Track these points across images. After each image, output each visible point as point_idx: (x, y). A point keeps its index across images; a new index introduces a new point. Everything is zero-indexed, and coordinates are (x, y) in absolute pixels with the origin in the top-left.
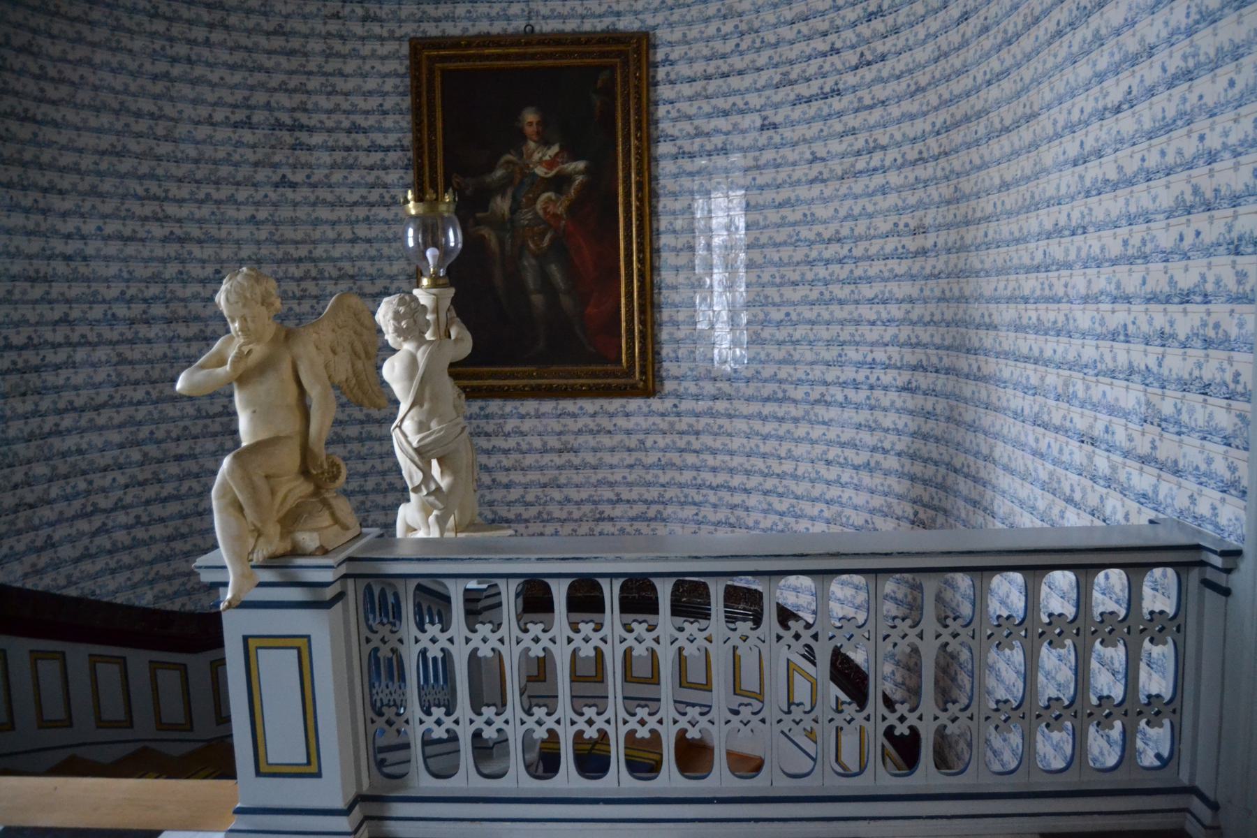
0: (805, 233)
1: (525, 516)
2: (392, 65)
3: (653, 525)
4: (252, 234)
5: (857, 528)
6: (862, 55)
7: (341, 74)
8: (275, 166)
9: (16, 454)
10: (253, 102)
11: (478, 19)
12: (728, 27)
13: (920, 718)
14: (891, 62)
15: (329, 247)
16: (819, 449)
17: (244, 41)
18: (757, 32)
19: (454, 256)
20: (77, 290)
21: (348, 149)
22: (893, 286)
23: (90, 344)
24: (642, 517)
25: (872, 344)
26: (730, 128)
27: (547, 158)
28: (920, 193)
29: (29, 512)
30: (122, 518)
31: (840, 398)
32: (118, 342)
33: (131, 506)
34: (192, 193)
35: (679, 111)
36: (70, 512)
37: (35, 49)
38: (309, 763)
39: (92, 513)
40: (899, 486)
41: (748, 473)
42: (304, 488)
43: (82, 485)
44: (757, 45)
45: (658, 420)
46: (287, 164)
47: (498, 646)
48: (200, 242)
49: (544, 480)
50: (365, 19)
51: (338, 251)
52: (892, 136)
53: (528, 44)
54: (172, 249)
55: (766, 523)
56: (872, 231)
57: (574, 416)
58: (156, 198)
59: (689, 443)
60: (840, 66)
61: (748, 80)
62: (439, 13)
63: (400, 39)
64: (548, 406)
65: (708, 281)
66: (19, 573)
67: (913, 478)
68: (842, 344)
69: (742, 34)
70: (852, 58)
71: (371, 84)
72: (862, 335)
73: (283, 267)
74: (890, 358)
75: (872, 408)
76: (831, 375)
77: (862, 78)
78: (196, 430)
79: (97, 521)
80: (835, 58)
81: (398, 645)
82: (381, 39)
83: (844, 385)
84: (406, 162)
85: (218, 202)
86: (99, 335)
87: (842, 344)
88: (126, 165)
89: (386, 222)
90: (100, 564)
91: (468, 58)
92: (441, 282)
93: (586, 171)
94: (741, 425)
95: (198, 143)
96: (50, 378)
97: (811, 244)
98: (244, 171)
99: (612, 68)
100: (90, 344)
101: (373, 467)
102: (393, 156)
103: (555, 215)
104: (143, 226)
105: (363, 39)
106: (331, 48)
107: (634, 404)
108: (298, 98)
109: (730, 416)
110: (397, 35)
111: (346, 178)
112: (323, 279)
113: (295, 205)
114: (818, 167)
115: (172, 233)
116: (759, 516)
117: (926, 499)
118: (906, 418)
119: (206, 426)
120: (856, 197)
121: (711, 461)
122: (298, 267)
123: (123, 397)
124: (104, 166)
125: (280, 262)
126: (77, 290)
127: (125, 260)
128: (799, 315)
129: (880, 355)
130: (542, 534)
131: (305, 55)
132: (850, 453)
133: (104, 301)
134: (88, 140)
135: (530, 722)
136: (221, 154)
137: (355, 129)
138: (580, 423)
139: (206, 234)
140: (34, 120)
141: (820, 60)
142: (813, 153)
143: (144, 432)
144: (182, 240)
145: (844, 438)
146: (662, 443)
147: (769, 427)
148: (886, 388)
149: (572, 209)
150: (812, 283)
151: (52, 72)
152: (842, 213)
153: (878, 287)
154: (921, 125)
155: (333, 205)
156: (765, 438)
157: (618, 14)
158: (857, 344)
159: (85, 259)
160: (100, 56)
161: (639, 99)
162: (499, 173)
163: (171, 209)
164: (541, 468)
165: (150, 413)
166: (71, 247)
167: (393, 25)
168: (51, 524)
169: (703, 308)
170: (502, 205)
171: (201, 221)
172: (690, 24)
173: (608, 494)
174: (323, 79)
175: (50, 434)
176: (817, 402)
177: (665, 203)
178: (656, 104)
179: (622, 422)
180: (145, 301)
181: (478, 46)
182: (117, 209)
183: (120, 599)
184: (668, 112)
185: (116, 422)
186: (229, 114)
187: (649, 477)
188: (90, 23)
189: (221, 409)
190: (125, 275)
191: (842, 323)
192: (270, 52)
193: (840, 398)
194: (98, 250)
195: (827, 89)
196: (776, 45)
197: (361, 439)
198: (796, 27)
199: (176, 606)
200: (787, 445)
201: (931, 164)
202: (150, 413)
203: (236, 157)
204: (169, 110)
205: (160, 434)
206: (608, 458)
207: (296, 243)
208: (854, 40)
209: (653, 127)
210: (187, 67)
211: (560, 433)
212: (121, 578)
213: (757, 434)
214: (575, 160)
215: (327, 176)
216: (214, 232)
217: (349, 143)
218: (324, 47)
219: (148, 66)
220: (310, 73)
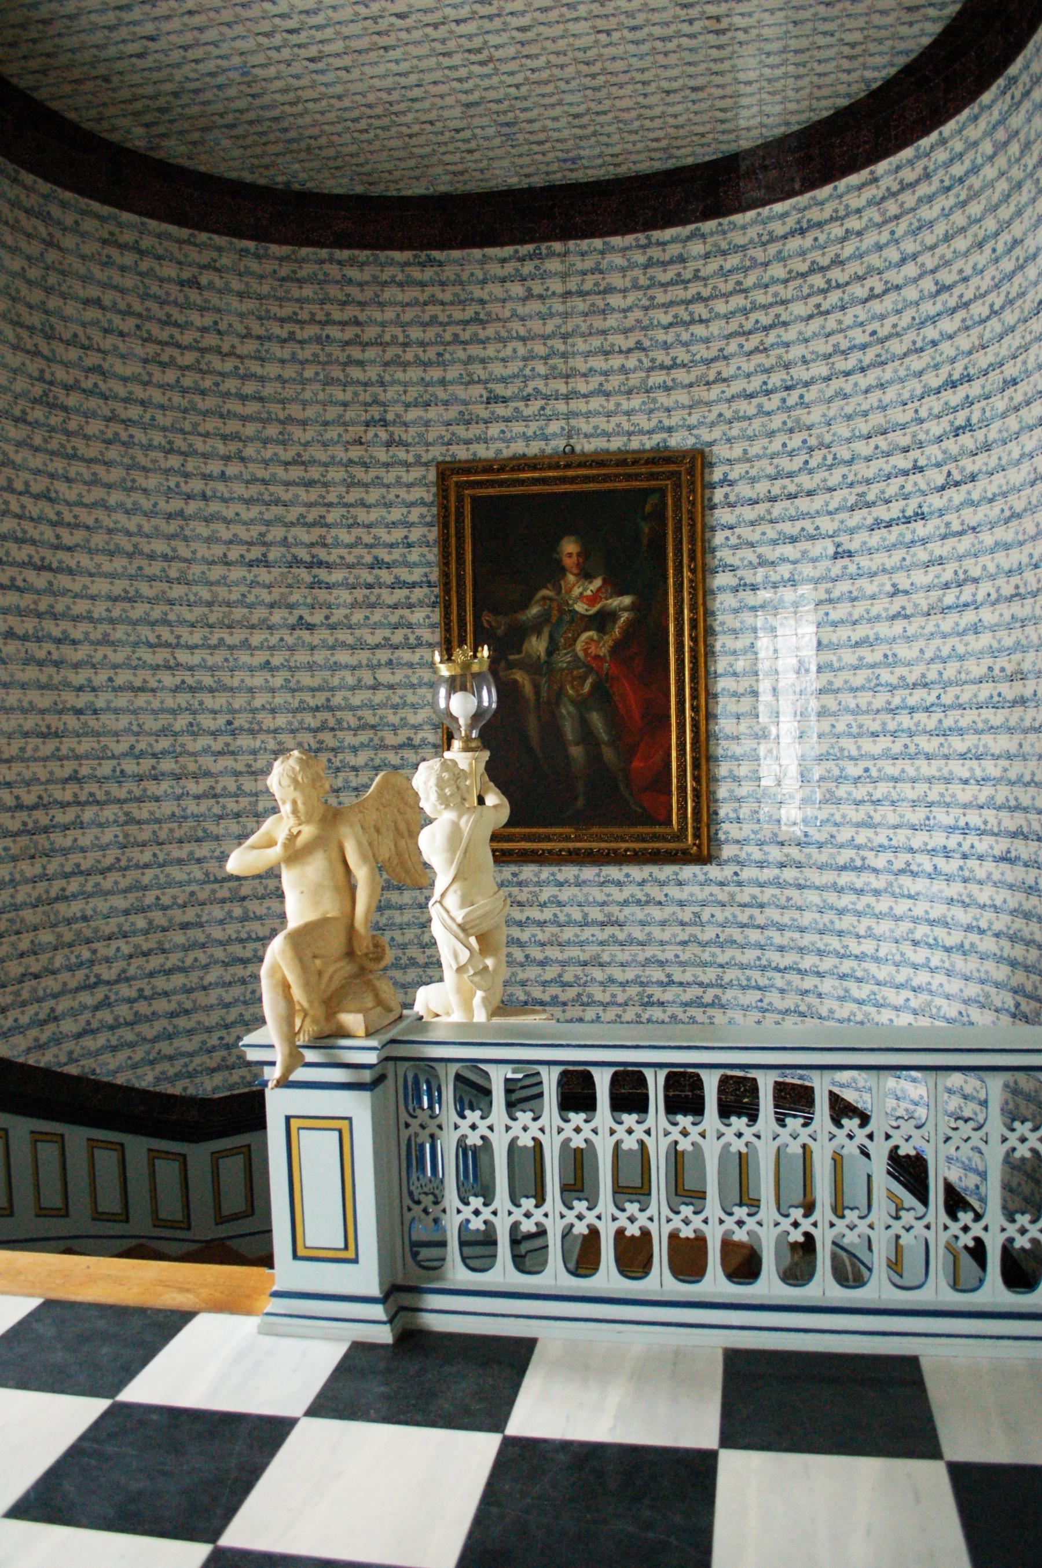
0: (886, 676)
1: (563, 998)
2: (418, 493)
3: (710, 1011)
5: (948, 1021)
6: (949, 474)
7: (363, 504)
8: (291, 607)
9: (23, 920)
10: (269, 538)
11: (512, 440)
12: (795, 442)
13: (986, 1229)
14: (982, 483)
15: (348, 694)
16: (905, 926)
17: (261, 473)
19: (488, 717)
20: (87, 745)
21: (369, 586)
22: (987, 739)
23: (98, 803)
24: (697, 1003)
25: (965, 806)
26: (799, 556)
28: (1017, 634)
29: (34, 982)
30: (125, 991)
31: (929, 868)
32: (125, 801)
33: (134, 978)
34: (205, 638)
36: (73, 984)
37: (53, 495)
38: (346, 1248)
39: (96, 985)
40: (1001, 973)
41: (820, 953)
42: (347, 969)
43: (86, 955)
44: (829, 462)
45: (715, 889)
48: (211, 690)
49: (583, 957)
52: (984, 568)
53: (568, 466)
55: (843, 1012)
56: (963, 676)
57: (619, 884)
58: (168, 645)
59: (751, 917)
60: (923, 486)
61: (818, 502)
62: (470, 435)
63: (426, 464)
64: (589, 872)
65: (773, 730)
66: (23, 1047)
67: (1013, 964)
68: (930, 805)
70: (938, 477)
71: (396, 514)
72: (953, 796)
73: (299, 716)
74: (985, 823)
75: (965, 881)
76: (918, 840)
77: (950, 500)
78: (203, 895)
79: (100, 993)
81: (437, 1131)
82: (407, 465)
83: (932, 852)
85: (231, 648)
86: (107, 793)
87: (930, 805)
88: (139, 611)
89: (411, 665)
90: (101, 1040)
91: (501, 483)
92: (474, 745)
94: (813, 897)
95: (212, 584)
96: (59, 839)
97: (893, 688)
100: (98, 803)
102: (418, 593)
103: (597, 657)
105: (387, 465)
106: (353, 477)
107: (688, 871)
109: (800, 887)
111: (367, 618)
113: (313, 648)
114: (900, 601)
115: (183, 682)
116: (835, 1005)
117: (1029, 988)
118: (1005, 893)
119: (213, 891)
120: (944, 636)
121: (778, 939)
123: (129, 860)
124: (116, 613)
125: (295, 711)
126: (87, 745)
127: (134, 712)
129: (974, 818)
130: (581, 1020)
132: (940, 932)
133: (113, 757)
134: (101, 586)
135: (571, 1216)
136: (235, 596)
137: (378, 564)
138: (627, 892)
139: (219, 681)
140: (50, 569)
141: (901, 480)
142: (894, 585)
143: (150, 898)
145: (933, 915)
146: (720, 915)
147: (847, 900)
148: (981, 858)
149: (616, 649)
150: (894, 734)
151: (68, 517)
152: (929, 654)
153: (970, 740)
154: (1016, 556)
155: (353, 648)
156: (841, 912)
157: (670, 430)
158: (948, 805)
159: (95, 712)
160: (115, 497)
161: (693, 526)
162: (535, 610)
163: (183, 657)
164: (581, 944)
165: (157, 877)
166: (82, 700)
167: (420, 450)
168: (55, 996)
169: (768, 761)
170: (537, 646)
172: (751, 439)
173: (658, 974)
174: (343, 511)
175: (57, 899)
176: (902, 872)
177: (722, 642)
178: (713, 529)
179: (674, 892)
180: (154, 755)
181: (512, 470)
182: (128, 658)
183: (120, 1080)
187: (706, 956)
188: (105, 463)
190: (135, 728)
191: (930, 780)
192: (288, 484)
193: (929, 868)
194: (109, 702)
195: (909, 512)
196: (850, 462)
198: (873, 442)
199: (177, 1090)
201: (1029, 601)
202: (157, 877)
203: (251, 598)
204: (184, 551)
205: (166, 900)
206: (657, 933)
208: (940, 457)
209: (708, 556)
210: (202, 504)
211: (604, 904)
212: (122, 1056)
213: (831, 908)
214: (621, 594)
215: (346, 617)
216: (227, 681)
217: (370, 579)
219: (162, 505)
220: (330, 505)
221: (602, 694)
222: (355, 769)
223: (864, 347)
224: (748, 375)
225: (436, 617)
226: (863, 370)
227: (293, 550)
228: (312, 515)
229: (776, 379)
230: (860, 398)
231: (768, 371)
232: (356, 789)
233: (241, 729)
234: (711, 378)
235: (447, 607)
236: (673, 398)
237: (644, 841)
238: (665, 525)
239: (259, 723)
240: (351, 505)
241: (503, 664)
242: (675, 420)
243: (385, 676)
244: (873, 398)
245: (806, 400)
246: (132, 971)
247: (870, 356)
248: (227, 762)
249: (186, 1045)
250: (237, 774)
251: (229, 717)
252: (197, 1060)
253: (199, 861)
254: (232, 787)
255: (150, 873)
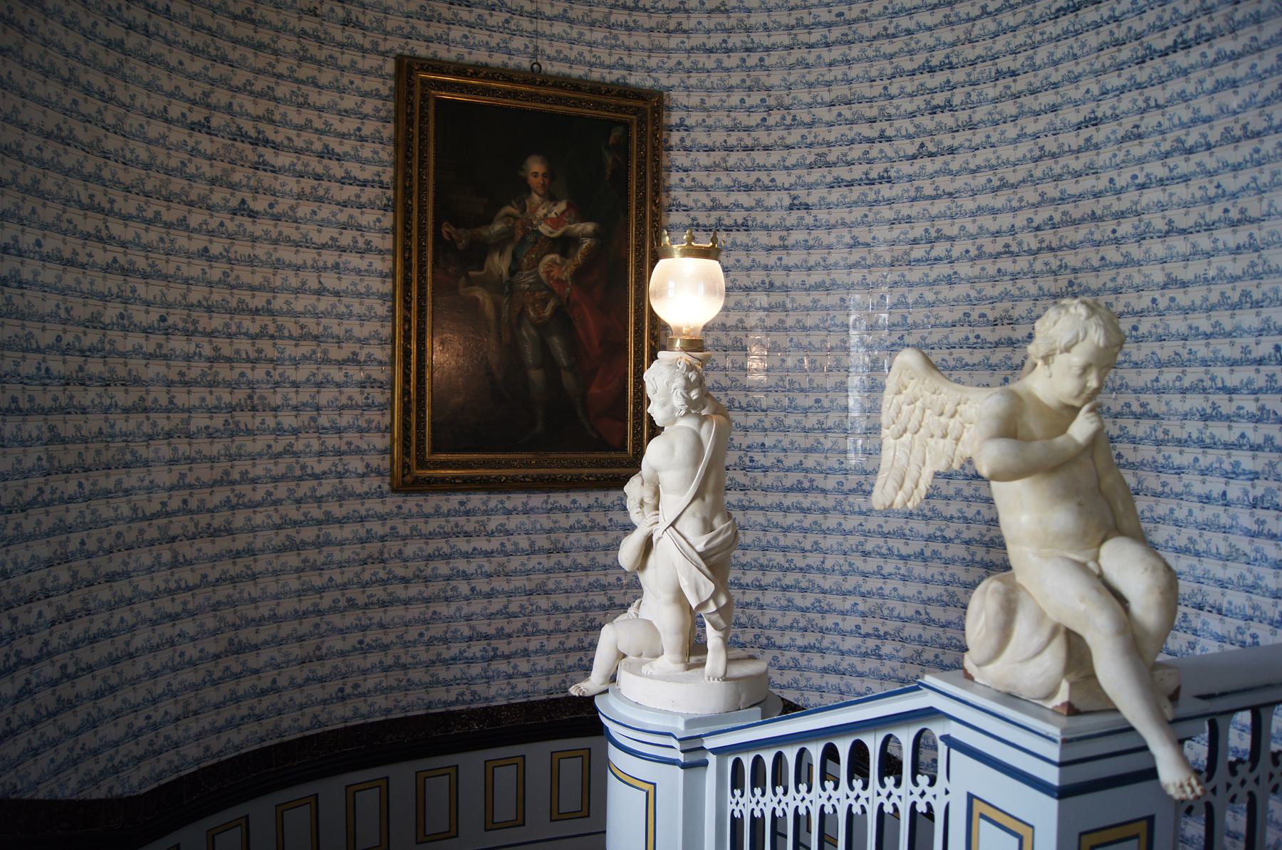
2: (372, 84)
4: (204, 272)
8: (233, 186)
10: (213, 100)
12: (754, 99)
16: (853, 540)
17: (208, 21)
18: (788, 109)
21: (318, 177)
27: (553, 215)
30: (48, 670)
32: (51, 411)
34: (140, 209)
35: (694, 180)
41: (762, 568)
46: (247, 186)
47: (881, 790)
48: (145, 276)
49: (529, 586)
50: (345, 23)
51: (301, 303)
54: (113, 283)
57: (566, 510)
58: (100, 210)
61: (775, 157)
63: (384, 54)
64: (537, 500)
69: (770, 109)
71: (349, 102)
73: (237, 318)
78: (130, 537)
80: (885, 146)
82: (362, 49)
84: (385, 201)
85: (168, 225)
89: (358, 272)
93: (595, 235)
98: (200, 188)
99: (627, 125)
101: (331, 579)
102: (370, 193)
103: (559, 281)
104: (84, 246)
105: (342, 45)
108: (263, 106)
110: (381, 48)
111: (314, 213)
112: (281, 338)
113: (254, 240)
115: (115, 260)
116: (777, 614)
119: (141, 531)
122: (253, 321)
123: (53, 491)
127: (62, 292)
128: (832, 401)
131: (276, 52)
133: (38, 350)
137: (326, 153)
139: (153, 266)
141: (866, 146)
142: (853, 238)
144: (126, 272)
147: (792, 519)
149: (579, 274)
155: (297, 244)
156: (786, 530)
157: (629, 68)
159: (21, 285)
162: (498, 227)
163: (116, 228)
164: (528, 573)
167: (378, 37)
170: (499, 263)
171: (147, 248)
174: (294, 86)
178: (669, 169)
180: (82, 352)
181: (486, 77)
183: (42, 794)
184: (682, 180)
185: (45, 527)
186: (185, 111)
189: (159, 507)
190: (63, 314)
192: (236, 41)
196: (810, 125)
197: (318, 545)
198: (835, 110)
200: (811, 538)
203: (191, 169)
204: (121, 94)
205: (91, 545)
207: (252, 288)
211: (550, 531)
213: (777, 526)
215: (292, 208)
217: (320, 170)
218: (298, 47)
220: (280, 76)
221: (563, 318)
222: (295, 385)
223: (829, 25)
224: (709, 31)
225: (388, 221)
226: (827, 45)
227: (238, 120)
228: (261, 84)
229: (736, 40)
230: (824, 70)
231: (729, 31)
232: (295, 408)
233: (175, 327)
234: (672, 27)
235: (407, 211)
236: (634, 39)
237: (603, 466)
238: (627, 158)
239: (195, 322)
240: (302, 82)
241: (463, 279)
242: (634, 60)
243: (330, 281)
244: (838, 72)
245: (767, 63)
246: (55, 642)
247: (835, 34)
248: (157, 368)
249: (110, 731)
250: (170, 384)
251: (163, 311)
252: (123, 750)
253: (127, 492)
254: (164, 401)
255: (75, 509)
